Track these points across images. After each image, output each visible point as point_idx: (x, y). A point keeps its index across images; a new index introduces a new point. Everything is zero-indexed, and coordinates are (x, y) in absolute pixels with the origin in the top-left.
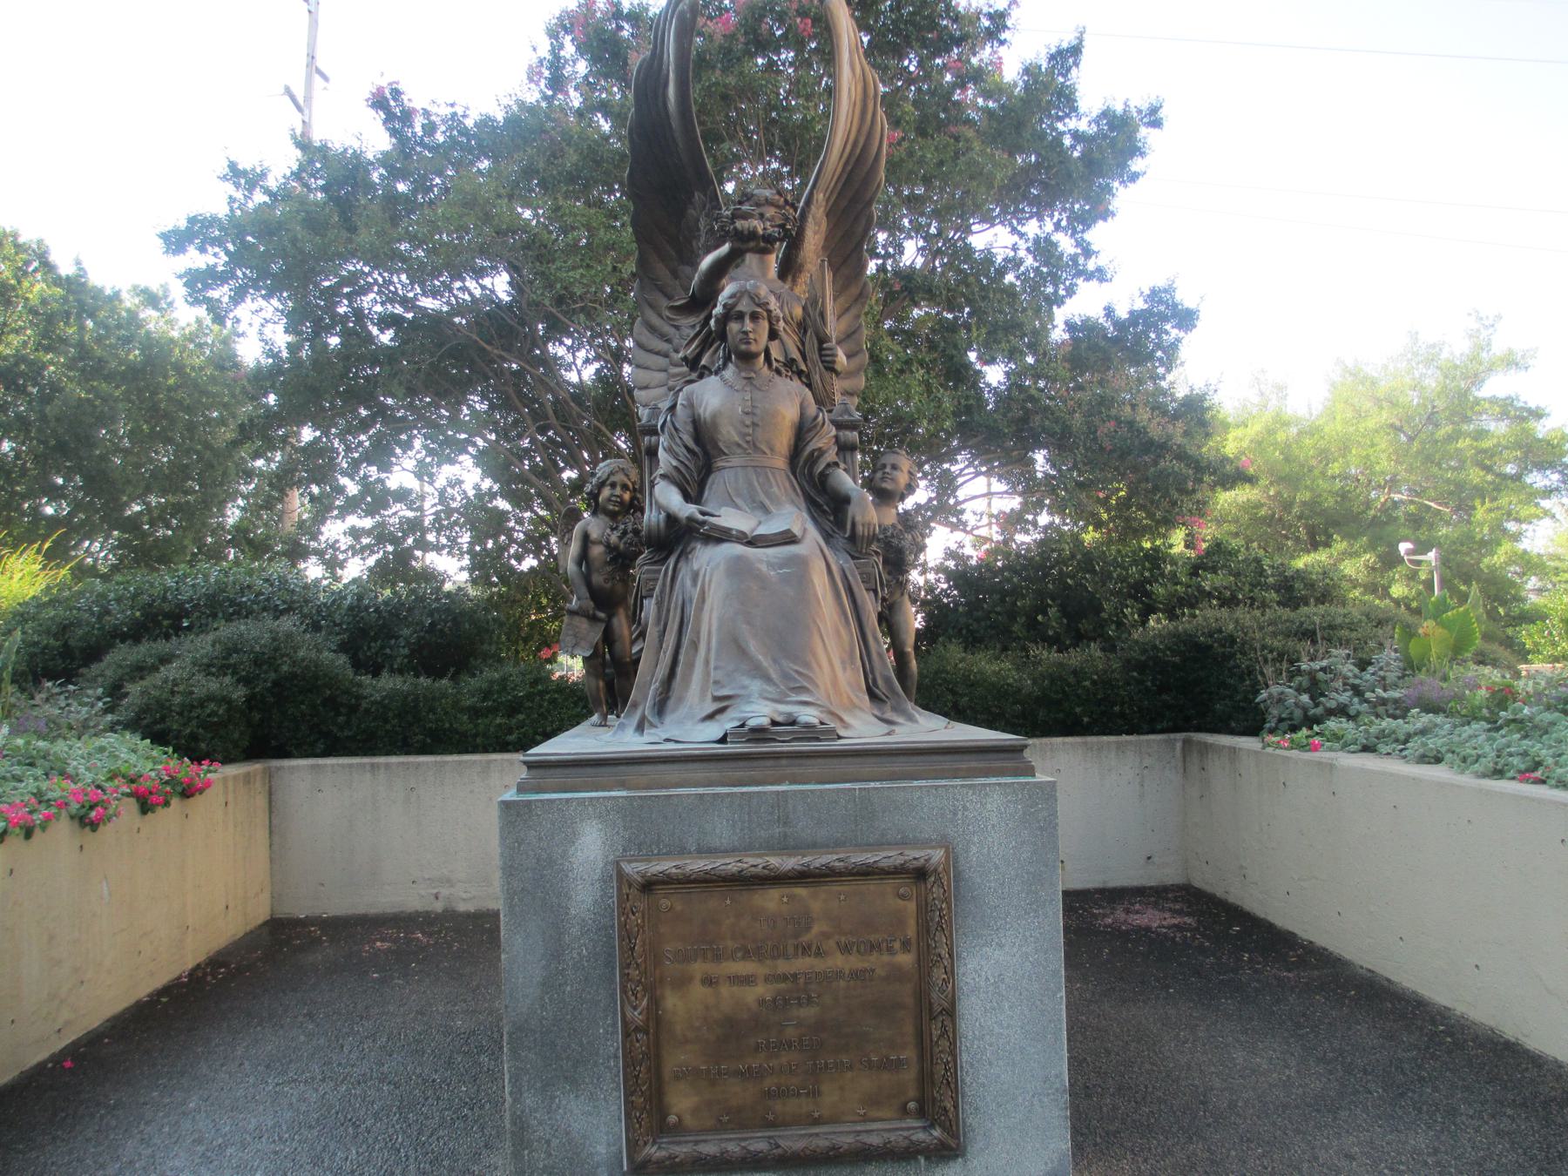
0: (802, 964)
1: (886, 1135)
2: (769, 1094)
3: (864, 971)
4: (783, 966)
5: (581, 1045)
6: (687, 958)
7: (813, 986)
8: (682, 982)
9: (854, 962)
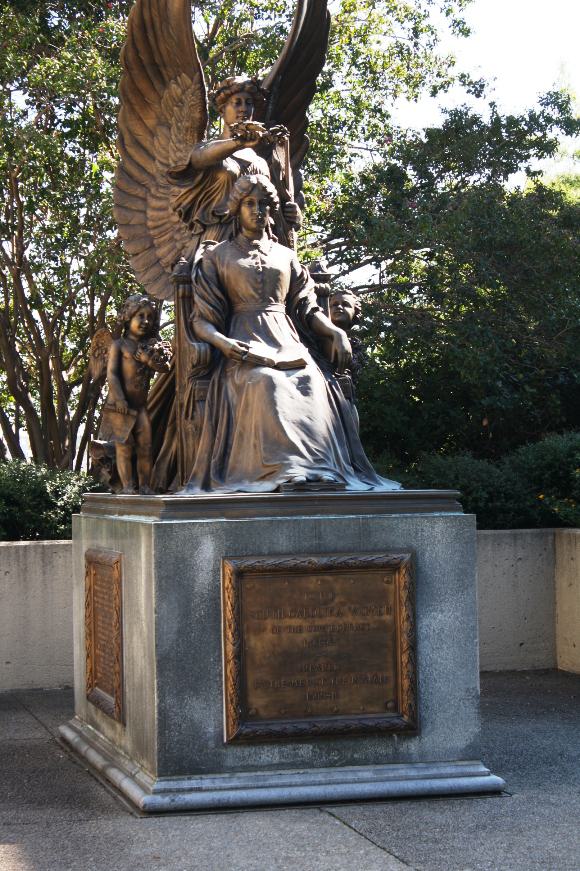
0: (328, 620)
3: (363, 624)
4: (319, 622)
5: (200, 668)
8: (260, 630)
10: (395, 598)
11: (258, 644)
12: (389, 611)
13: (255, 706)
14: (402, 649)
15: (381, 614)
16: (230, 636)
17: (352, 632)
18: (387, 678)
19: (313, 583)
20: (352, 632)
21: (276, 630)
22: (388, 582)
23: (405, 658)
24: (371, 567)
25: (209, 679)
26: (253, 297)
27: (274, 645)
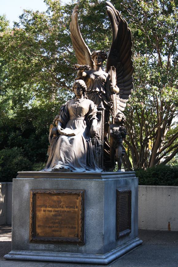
4: (56, 209)
6: (41, 206)
8: (40, 211)
11: (40, 214)
15: (74, 208)
19: (55, 198)
21: (44, 211)
26: (73, 115)
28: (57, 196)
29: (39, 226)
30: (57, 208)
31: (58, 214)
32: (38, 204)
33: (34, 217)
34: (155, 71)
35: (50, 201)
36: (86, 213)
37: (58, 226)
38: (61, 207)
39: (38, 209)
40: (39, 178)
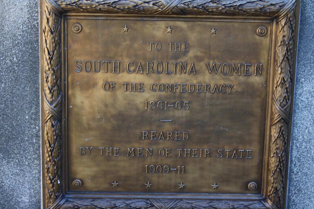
0: (178, 78)
1: (231, 203)
2: (150, 169)
3: (225, 86)
4: (165, 80)
5: (12, 127)
6: (92, 68)
7: (186, 95)
8: (89, 86)
9: (217, 80)
10: (269, 55)
11: (87, 102)
12: (259, 71)
13: (79, 176)
14: (272, 119)
15: (248, 74)
16: (48, 92)
17: (208, 95)
18: (250, 154)
19: (159, 29)
20: (208, 95)
21: (110, 86)
22: (261, 35)
23: (275, 132)
24: (239, 14)
25: (23, 140)
27: (106, 106)
28: (171, 23)
29: (84, 152)
30: (168, 73)
31: (173, 97)
32: (78, 58)
33: (62, 114)
34: (29, 48)
35: (136, 45)
36: (300, 95)
37: (170, 151)
38: (188, 68)
39: (77, 76)
40: (191, 201)
